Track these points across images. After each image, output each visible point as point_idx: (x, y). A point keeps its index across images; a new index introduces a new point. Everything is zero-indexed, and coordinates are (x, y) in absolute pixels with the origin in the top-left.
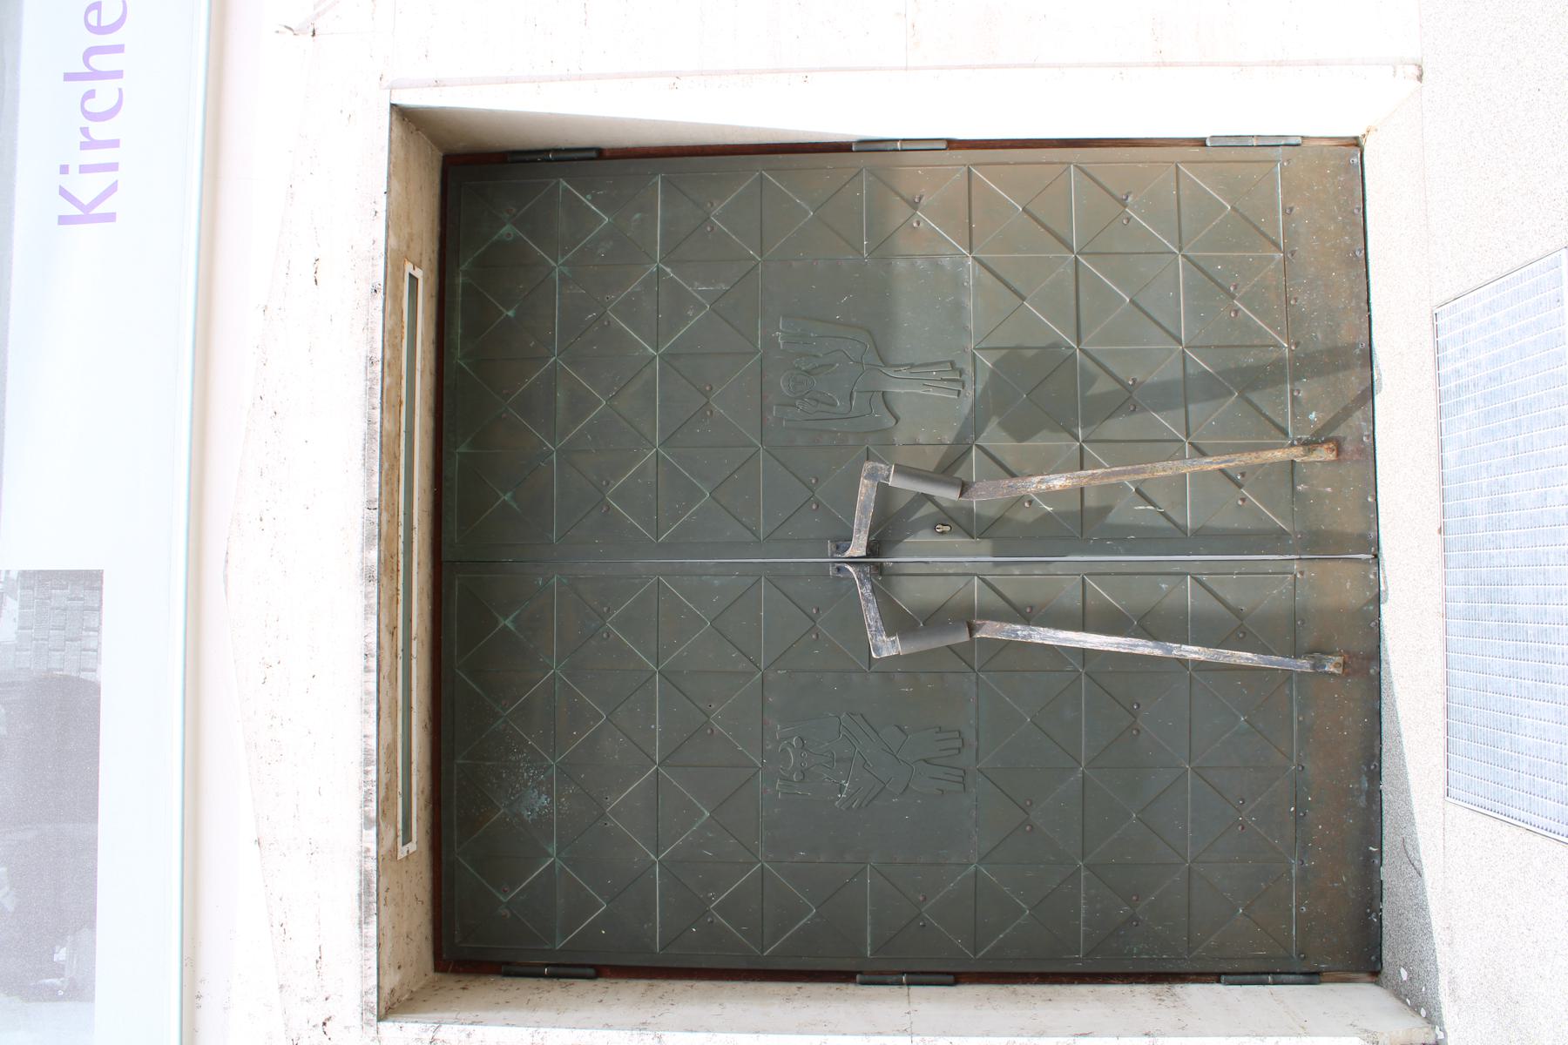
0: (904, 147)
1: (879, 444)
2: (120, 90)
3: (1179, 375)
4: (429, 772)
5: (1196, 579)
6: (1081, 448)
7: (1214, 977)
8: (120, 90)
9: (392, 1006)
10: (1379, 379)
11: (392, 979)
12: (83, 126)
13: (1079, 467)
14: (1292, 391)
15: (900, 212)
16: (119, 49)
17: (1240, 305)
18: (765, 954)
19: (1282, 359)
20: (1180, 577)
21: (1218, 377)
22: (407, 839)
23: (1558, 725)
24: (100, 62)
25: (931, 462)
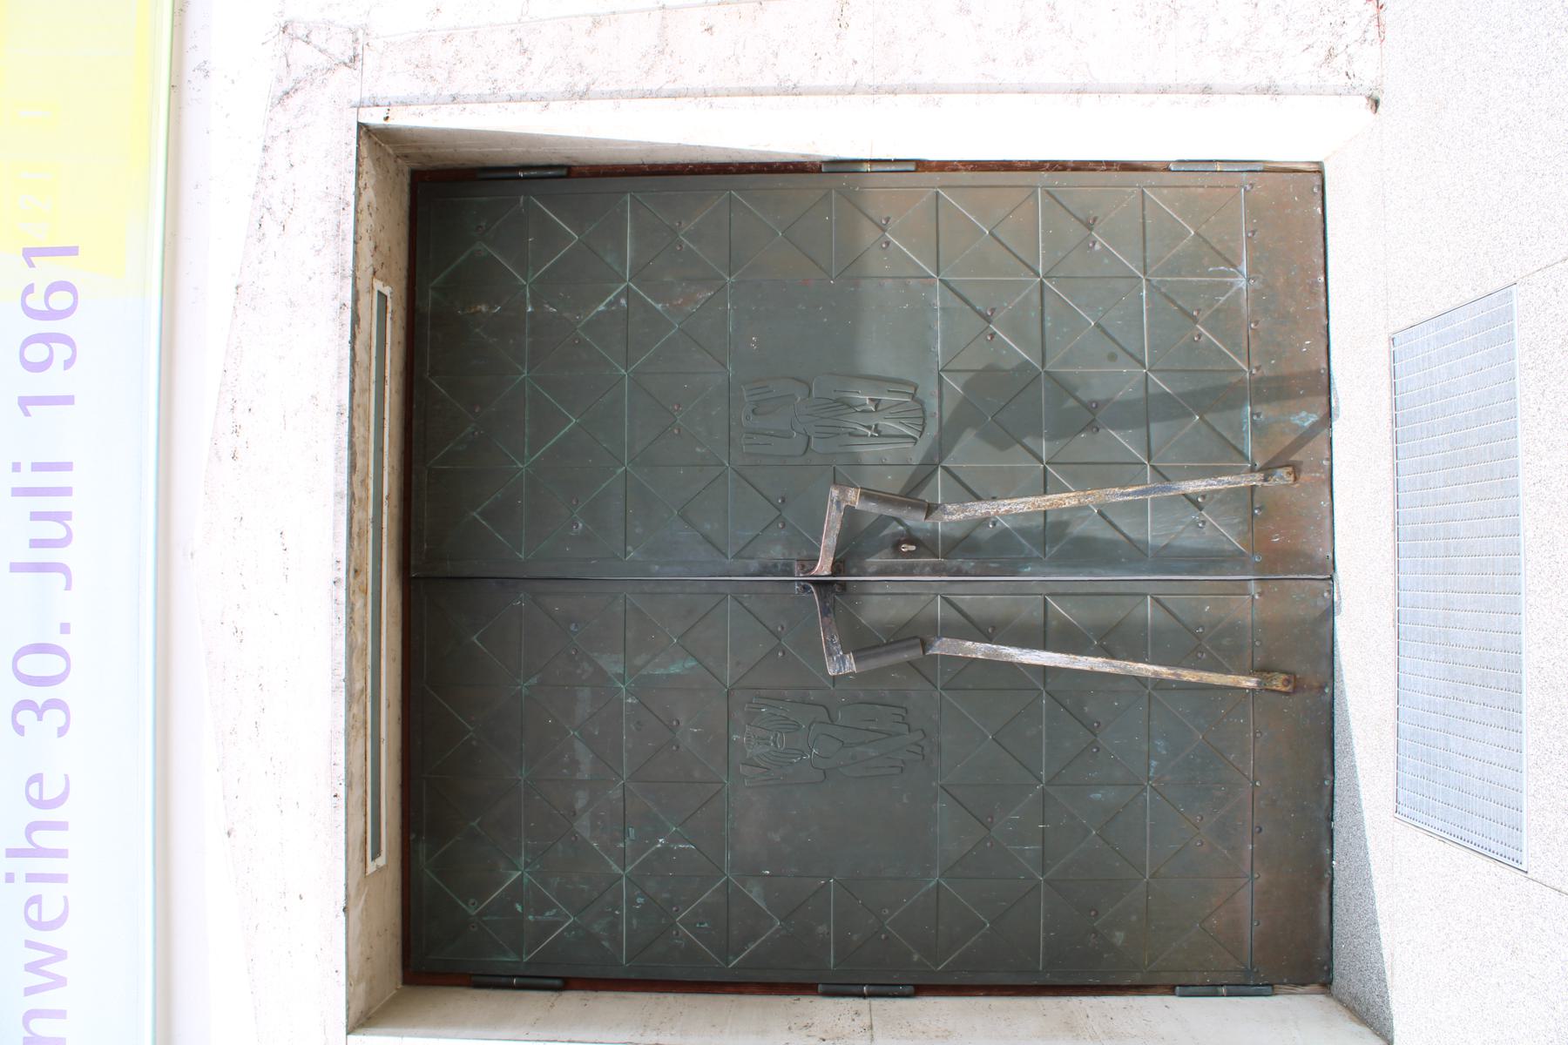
0: (874, 169)
1: (844, 472)
2: (66, 898)
3: (1141, 394)
4: (400, 763)
5: (1157, 601)
6: (1045, 468)
7: (1170, 989)
8: (66, 898)
9: (363, 1019)
10: (1338, 407)
11: (359, 1005)
12: (36, 288)
13: (1048, 513)
14: (1252, 414)
15: (869, 234)
16: (61, 826)
17: (1202, 330)
18: (730, 966)
19: (1242, 381)
20: (1142, 598)
21: (1180, 400)
22: (376, 853)
23: (1515, 792)
24: (43, 838)
25: (892, 482)
